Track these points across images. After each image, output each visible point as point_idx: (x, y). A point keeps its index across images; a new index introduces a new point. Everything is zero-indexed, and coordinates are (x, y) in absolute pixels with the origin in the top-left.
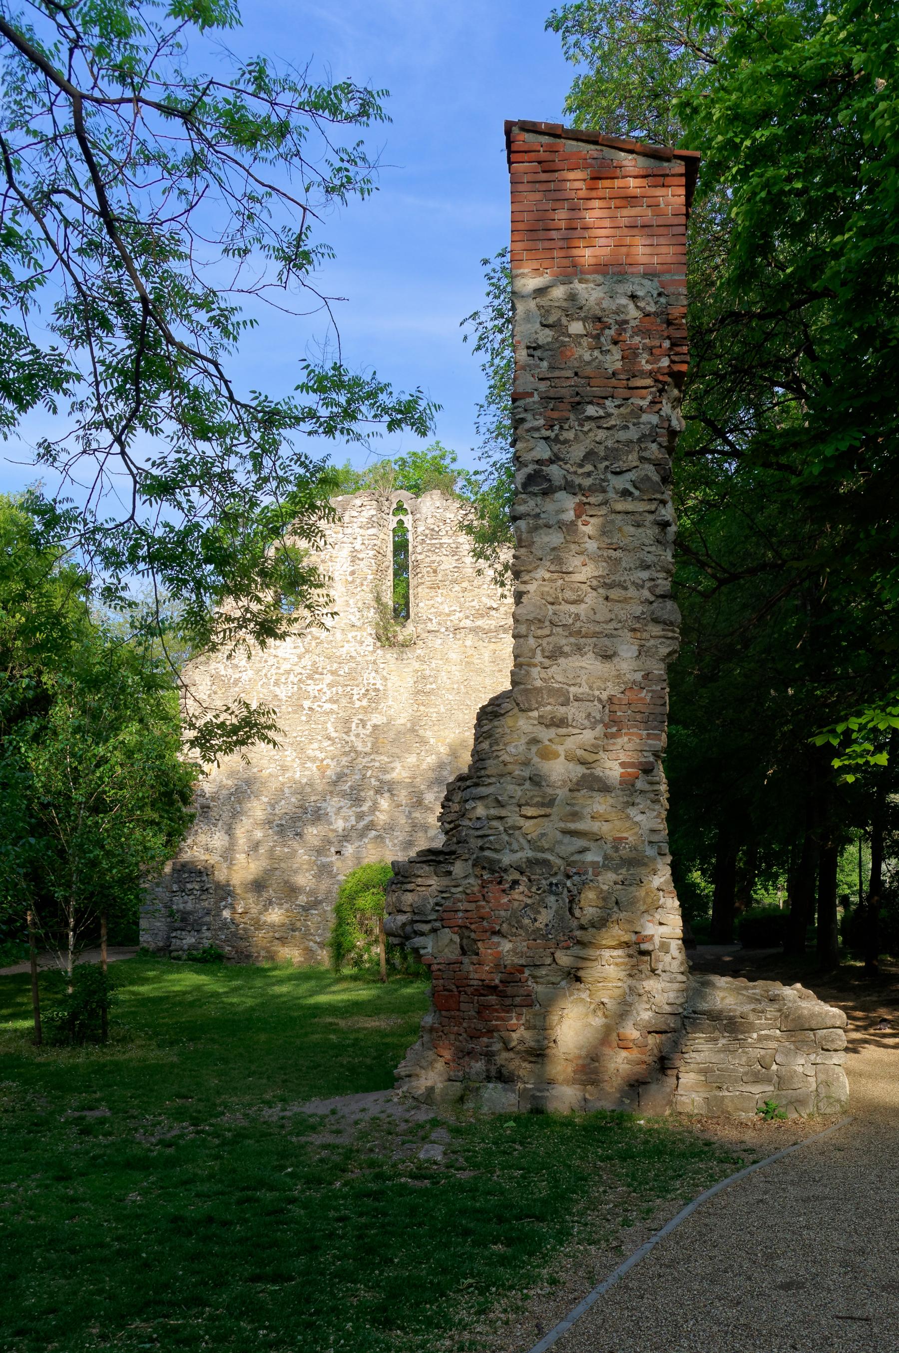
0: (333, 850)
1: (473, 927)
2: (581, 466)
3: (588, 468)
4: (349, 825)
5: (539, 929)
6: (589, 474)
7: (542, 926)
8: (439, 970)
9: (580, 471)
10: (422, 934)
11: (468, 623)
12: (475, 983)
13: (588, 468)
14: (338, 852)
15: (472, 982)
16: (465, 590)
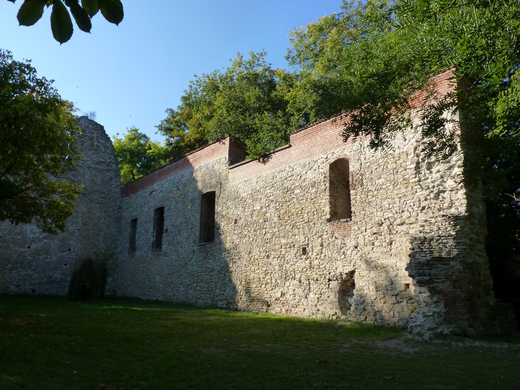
0: (27, 246)
4: (36, 236)
10: (436, 282)
11: (93, 166)
14: (29, 247)
16: (93, 154)
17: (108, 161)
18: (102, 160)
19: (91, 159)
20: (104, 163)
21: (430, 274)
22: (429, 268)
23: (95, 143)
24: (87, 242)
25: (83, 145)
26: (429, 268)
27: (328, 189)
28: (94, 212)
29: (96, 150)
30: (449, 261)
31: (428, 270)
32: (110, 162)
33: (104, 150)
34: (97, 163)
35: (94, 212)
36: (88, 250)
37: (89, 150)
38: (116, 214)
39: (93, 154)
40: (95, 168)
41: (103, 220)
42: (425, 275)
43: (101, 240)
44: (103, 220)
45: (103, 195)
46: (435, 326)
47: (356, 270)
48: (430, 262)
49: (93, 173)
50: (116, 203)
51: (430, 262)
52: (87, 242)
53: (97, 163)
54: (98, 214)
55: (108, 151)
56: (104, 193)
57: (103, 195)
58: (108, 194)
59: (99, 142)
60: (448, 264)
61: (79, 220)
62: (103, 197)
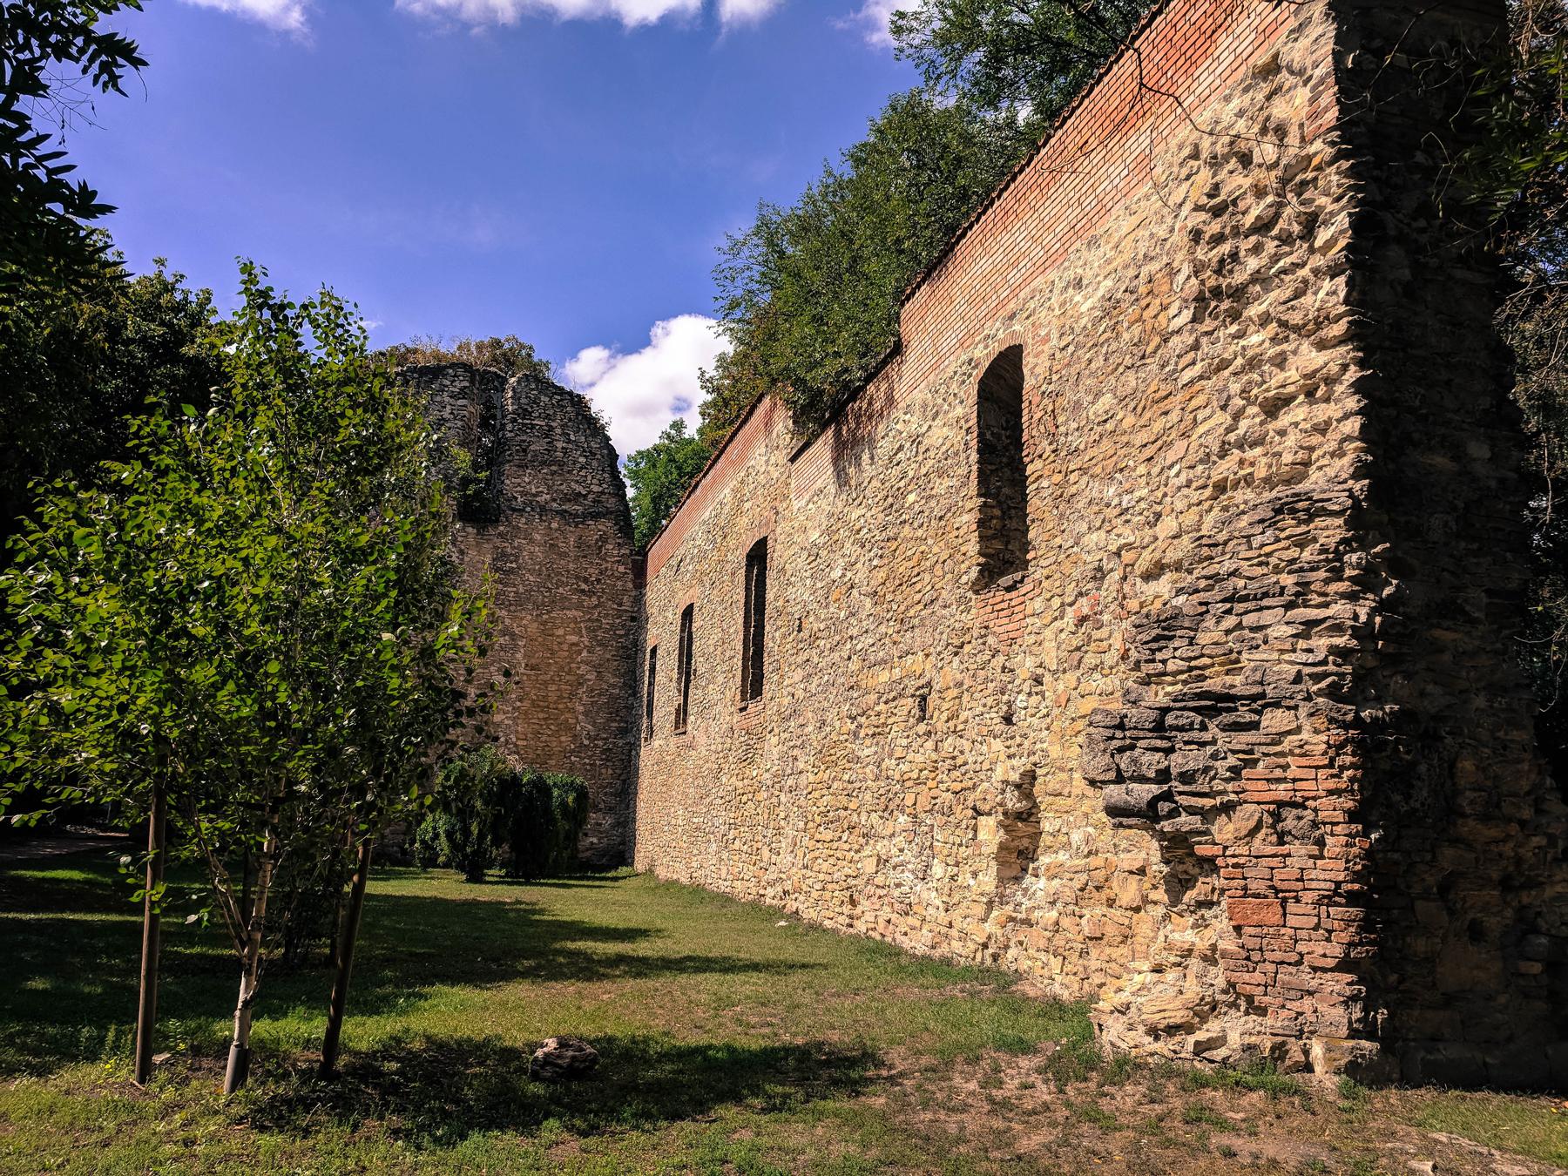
1: (1310, 803)
2: (1415, 219)
3: (1422, 223)
5: (1415, 810)
6: (1423, 231)
7: (1418, 805)
8: (1235, 866)
9: (1415, 225)
12: (1323, 885)
13: (1422, 223)
15: (1314, 885)
16: (553, 473)
17: (596, 489)
18: (578, 488)
19: (549, 488)
20: (585, 496)
21: (1163, 776)
22: (1159, 743)
23: (560, 445)
24: (541, 715)
25: (524, 451)
26: (1159, 743)
27: (974, 475)
28: (561, 632)
29: (561, 465)
30: (1259, 713)
31: (1158, 755)
32: (603, 493)
33: (582, 460)
34: (567, 499)
35: (561, 632)
36: (544, 738)
37: (543, 463)
38: (621, 636)
39: (553, 473)
40: (562, 513)
41: (585, 654)
42: (1143, 779)
43: (581, 709)
44: (585, 654)
45: (584, 586)
46: (1178, 1017)
47: (1039, 772)
48: (1170, 720)
49: (554, 525)
50: (620, 605)
51: (1170, 720)
52: (541, 715)
53: (567, 499)
54: (574, 639)
55: (595, 464)
56: (586, 580)
57: (584, 586)
58: (598, 581)
59: (569, 441)
60: (1254, 726)
61: (519, 656)
62: (583, 591)
